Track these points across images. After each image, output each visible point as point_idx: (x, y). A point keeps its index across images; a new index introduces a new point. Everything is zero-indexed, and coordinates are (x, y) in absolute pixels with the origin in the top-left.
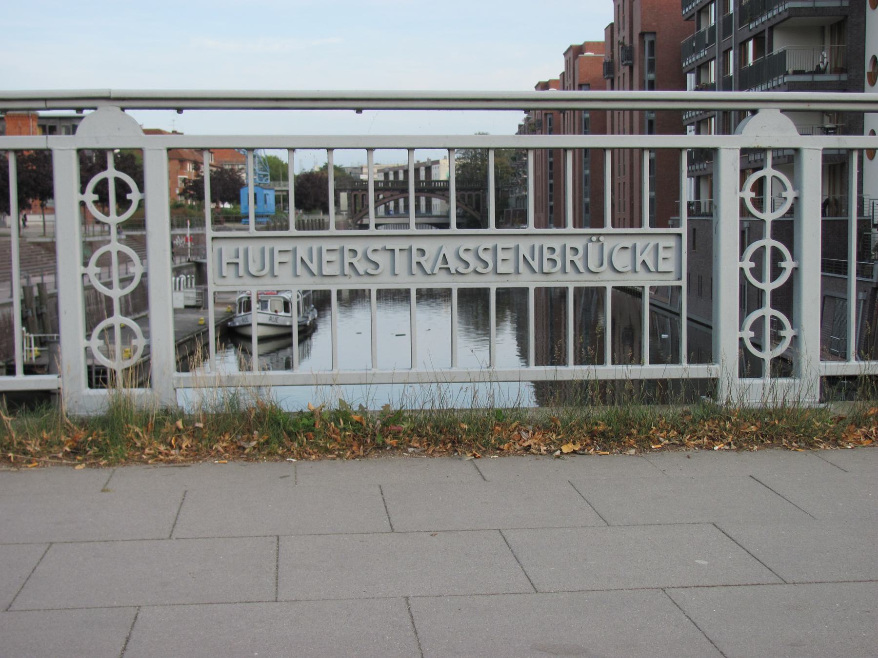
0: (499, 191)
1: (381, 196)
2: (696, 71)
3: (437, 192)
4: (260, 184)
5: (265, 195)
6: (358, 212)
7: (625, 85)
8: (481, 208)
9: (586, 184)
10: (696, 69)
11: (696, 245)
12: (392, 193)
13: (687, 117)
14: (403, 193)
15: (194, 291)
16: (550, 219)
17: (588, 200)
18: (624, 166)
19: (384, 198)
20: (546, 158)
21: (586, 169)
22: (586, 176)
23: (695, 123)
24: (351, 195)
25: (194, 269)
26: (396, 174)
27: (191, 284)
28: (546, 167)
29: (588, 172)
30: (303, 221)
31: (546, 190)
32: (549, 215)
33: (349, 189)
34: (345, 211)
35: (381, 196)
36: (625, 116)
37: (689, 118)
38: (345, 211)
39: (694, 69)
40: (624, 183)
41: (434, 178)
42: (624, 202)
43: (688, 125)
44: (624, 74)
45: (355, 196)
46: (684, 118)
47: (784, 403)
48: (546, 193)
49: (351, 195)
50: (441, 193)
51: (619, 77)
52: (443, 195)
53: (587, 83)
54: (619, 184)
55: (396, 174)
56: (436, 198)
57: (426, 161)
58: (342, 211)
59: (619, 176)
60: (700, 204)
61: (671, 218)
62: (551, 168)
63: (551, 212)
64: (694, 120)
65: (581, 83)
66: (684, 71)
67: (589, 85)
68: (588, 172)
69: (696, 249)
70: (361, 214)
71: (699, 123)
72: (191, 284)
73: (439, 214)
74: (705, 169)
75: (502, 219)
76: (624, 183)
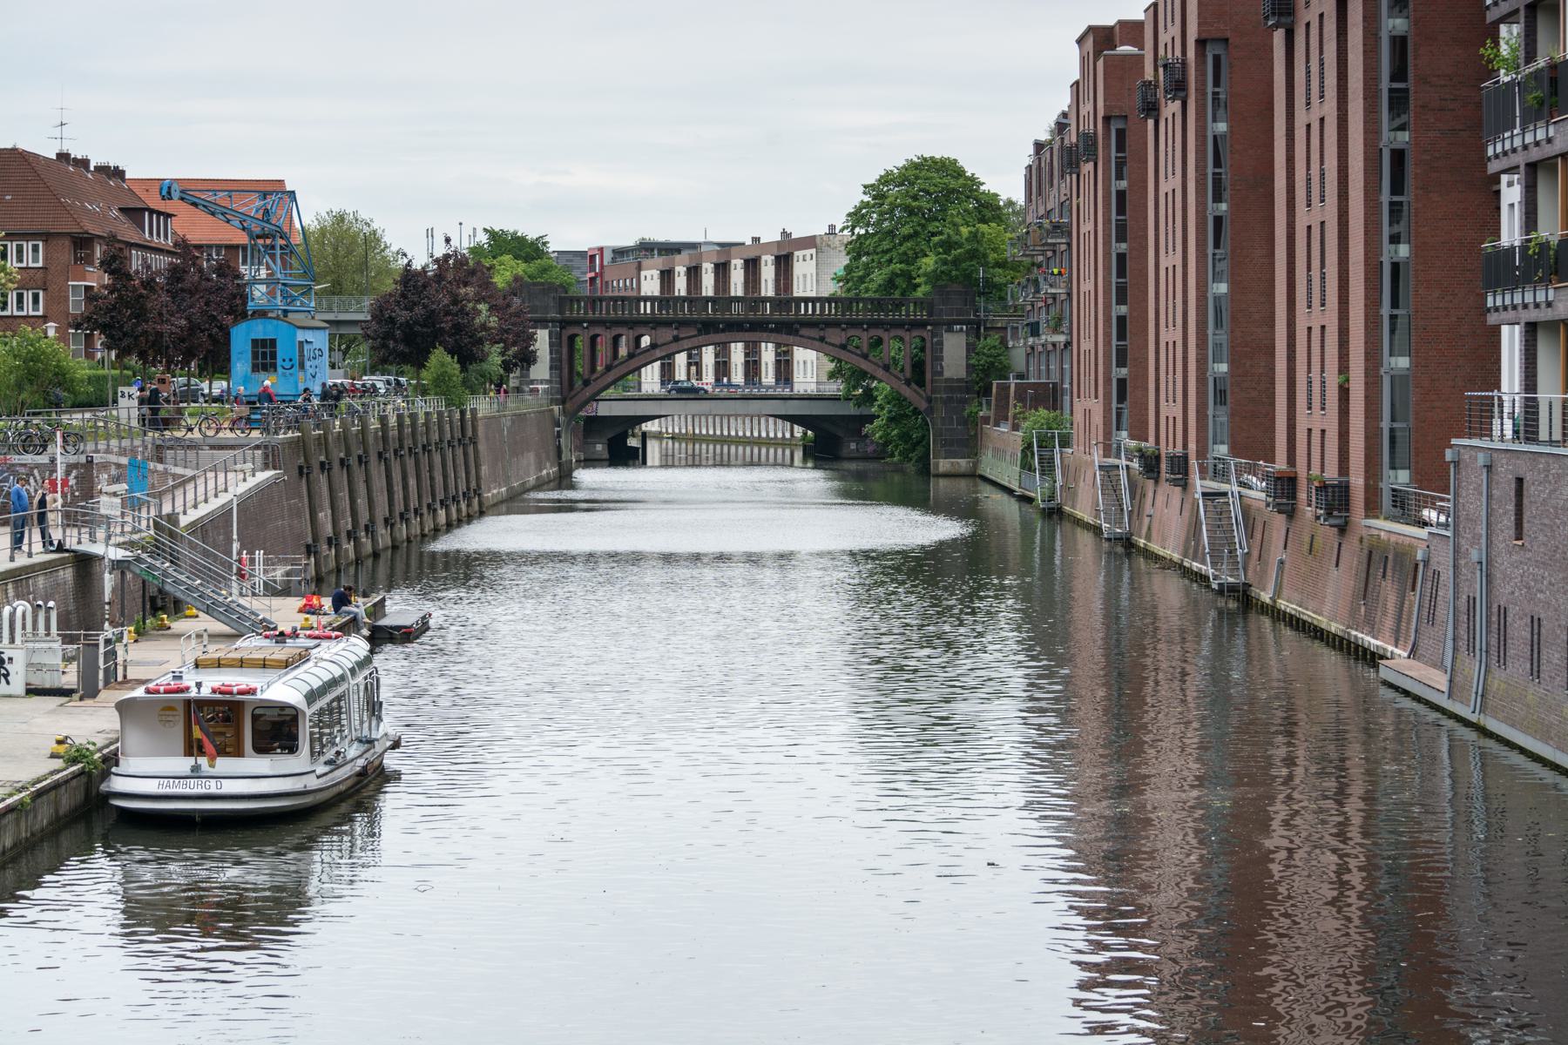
0: (979, 328)
1: (646, 341)
2: (1522, 20)
3: (804, 332)
4: (286, 312)
5: (301, 343)
6: (579, 383)
7: (1325, 48)
8: (928, 376)
9: (1218, 323)
10: (1522, 13)
11: (1526, 525)
12: (675, 332)
13: (1499, 149)
14: (707, 333)
15: (57, 645)
16: (1119, 415)
17: (1223, 368)
18: (1322, 175)
19: (653, 346)
20: (1107, 243)
21: (1217, 278)
22: (1217, 298)
23: (1522, 168)
24: (560, 336)
25: (67, 575)
26: (752, 266)
27: (48, 628)
28: (1107, 268)
29: (1223, 288)
30: (413, 417)
31: (1107, 335)
32: (1114, 405)
33: (553, 321)
34: (542, 382)
35: (646, 341)
36: (1325, 30)
37: (1505, 153)
38: (542, 382)
39: (1517, 11)
40: (1323, 327)
41: (798, 291)
42: (1323, 382)
43: (1505, 171)
44: (1321, 16)
45: (572, 338)
46: (1490, 152)
47: (1547, 290)
48: (1107, 343)
49: (560, 336)
50: (814, 333)
51: (1308, 25)
52: (822, 339)
53: (1219, 35)
54: (1310, 329)
55: (752, 266)
56: (806, 347)
57: (778, 238)
58: (532, 382)
59: (1310, 408)
60: (1537, 407)
61: (1454, 441)
62: (1121, 272)
63: (1122, 397)
64: (1520, 159)
65: (1204, 36)
66: (1491, 16)
67: (1226, 40)
68: (1223, 288)
69: (1525, 537)
70: (588, 392)
71: (1532, 168)
72: (48, 628)
73: (812, 389)
74: (1549, 304)
75: (989, 408)
76: (1323, 327)
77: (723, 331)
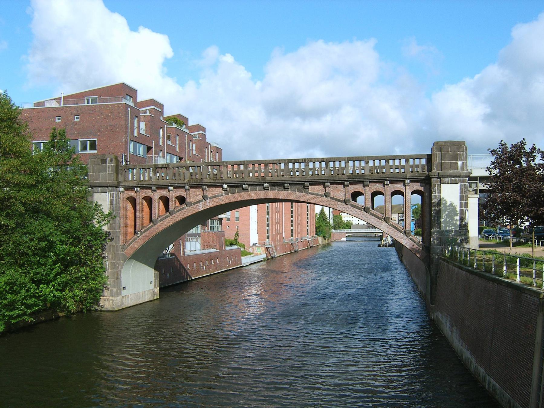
77: (245, 190)
